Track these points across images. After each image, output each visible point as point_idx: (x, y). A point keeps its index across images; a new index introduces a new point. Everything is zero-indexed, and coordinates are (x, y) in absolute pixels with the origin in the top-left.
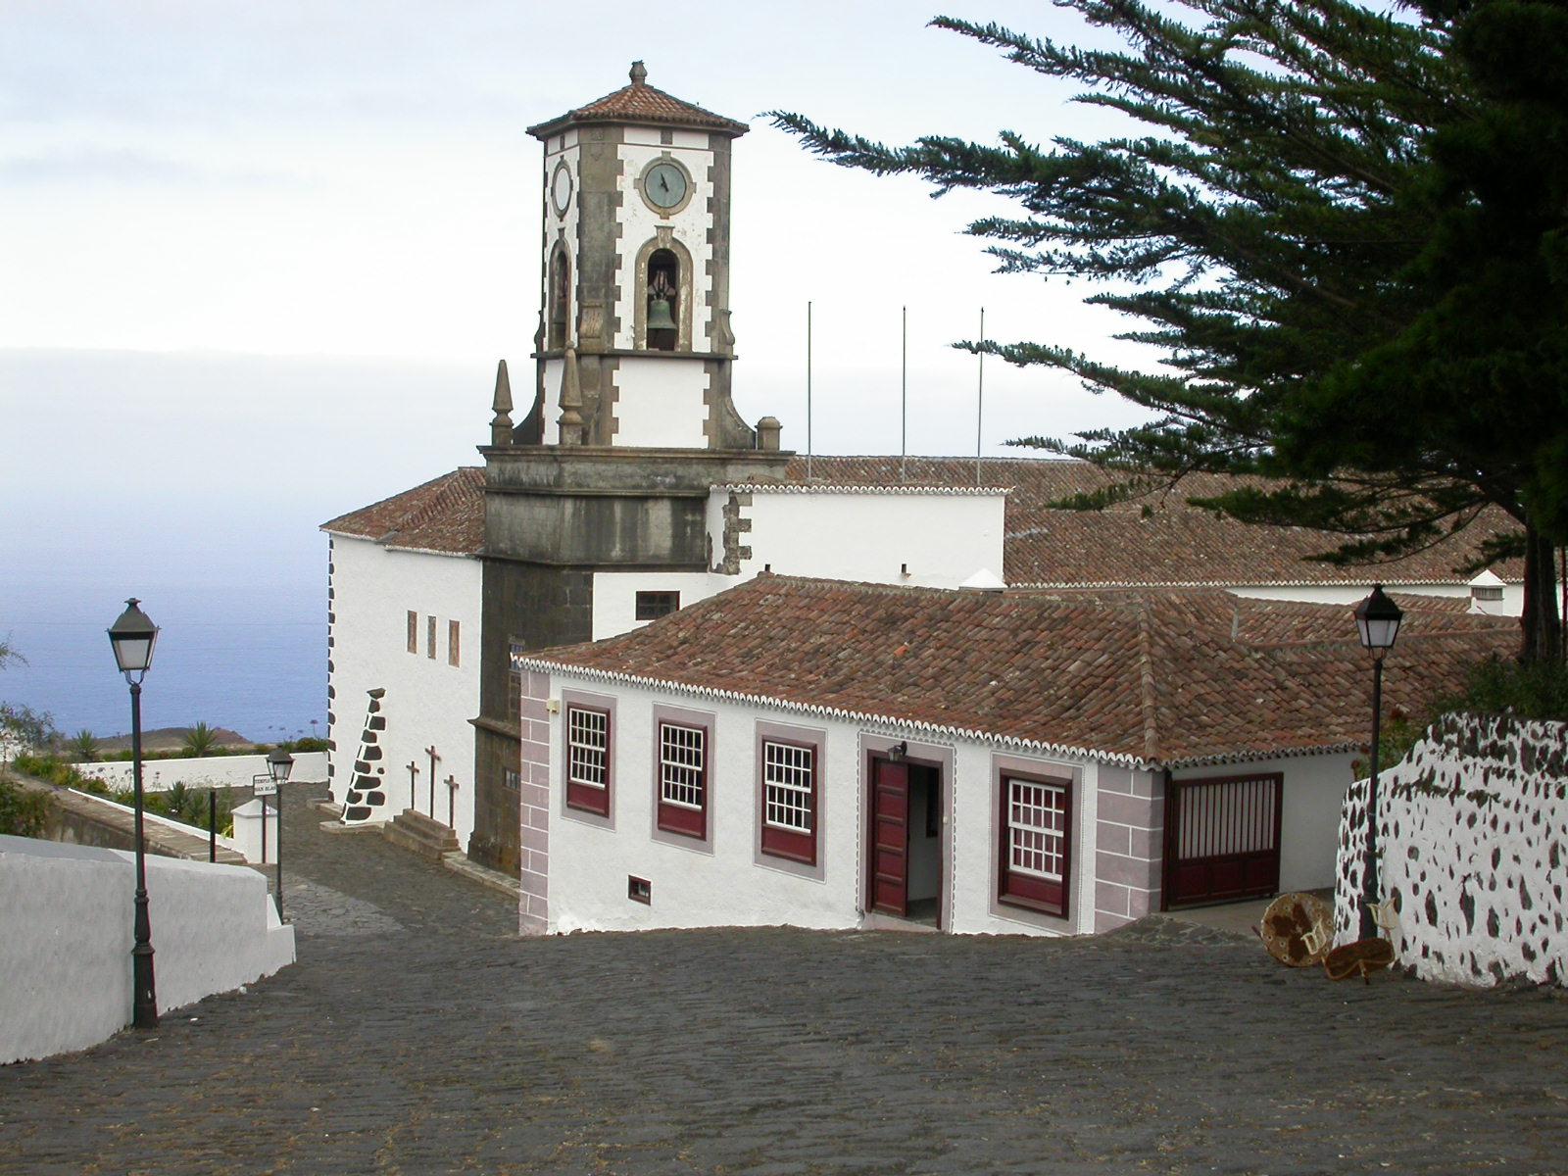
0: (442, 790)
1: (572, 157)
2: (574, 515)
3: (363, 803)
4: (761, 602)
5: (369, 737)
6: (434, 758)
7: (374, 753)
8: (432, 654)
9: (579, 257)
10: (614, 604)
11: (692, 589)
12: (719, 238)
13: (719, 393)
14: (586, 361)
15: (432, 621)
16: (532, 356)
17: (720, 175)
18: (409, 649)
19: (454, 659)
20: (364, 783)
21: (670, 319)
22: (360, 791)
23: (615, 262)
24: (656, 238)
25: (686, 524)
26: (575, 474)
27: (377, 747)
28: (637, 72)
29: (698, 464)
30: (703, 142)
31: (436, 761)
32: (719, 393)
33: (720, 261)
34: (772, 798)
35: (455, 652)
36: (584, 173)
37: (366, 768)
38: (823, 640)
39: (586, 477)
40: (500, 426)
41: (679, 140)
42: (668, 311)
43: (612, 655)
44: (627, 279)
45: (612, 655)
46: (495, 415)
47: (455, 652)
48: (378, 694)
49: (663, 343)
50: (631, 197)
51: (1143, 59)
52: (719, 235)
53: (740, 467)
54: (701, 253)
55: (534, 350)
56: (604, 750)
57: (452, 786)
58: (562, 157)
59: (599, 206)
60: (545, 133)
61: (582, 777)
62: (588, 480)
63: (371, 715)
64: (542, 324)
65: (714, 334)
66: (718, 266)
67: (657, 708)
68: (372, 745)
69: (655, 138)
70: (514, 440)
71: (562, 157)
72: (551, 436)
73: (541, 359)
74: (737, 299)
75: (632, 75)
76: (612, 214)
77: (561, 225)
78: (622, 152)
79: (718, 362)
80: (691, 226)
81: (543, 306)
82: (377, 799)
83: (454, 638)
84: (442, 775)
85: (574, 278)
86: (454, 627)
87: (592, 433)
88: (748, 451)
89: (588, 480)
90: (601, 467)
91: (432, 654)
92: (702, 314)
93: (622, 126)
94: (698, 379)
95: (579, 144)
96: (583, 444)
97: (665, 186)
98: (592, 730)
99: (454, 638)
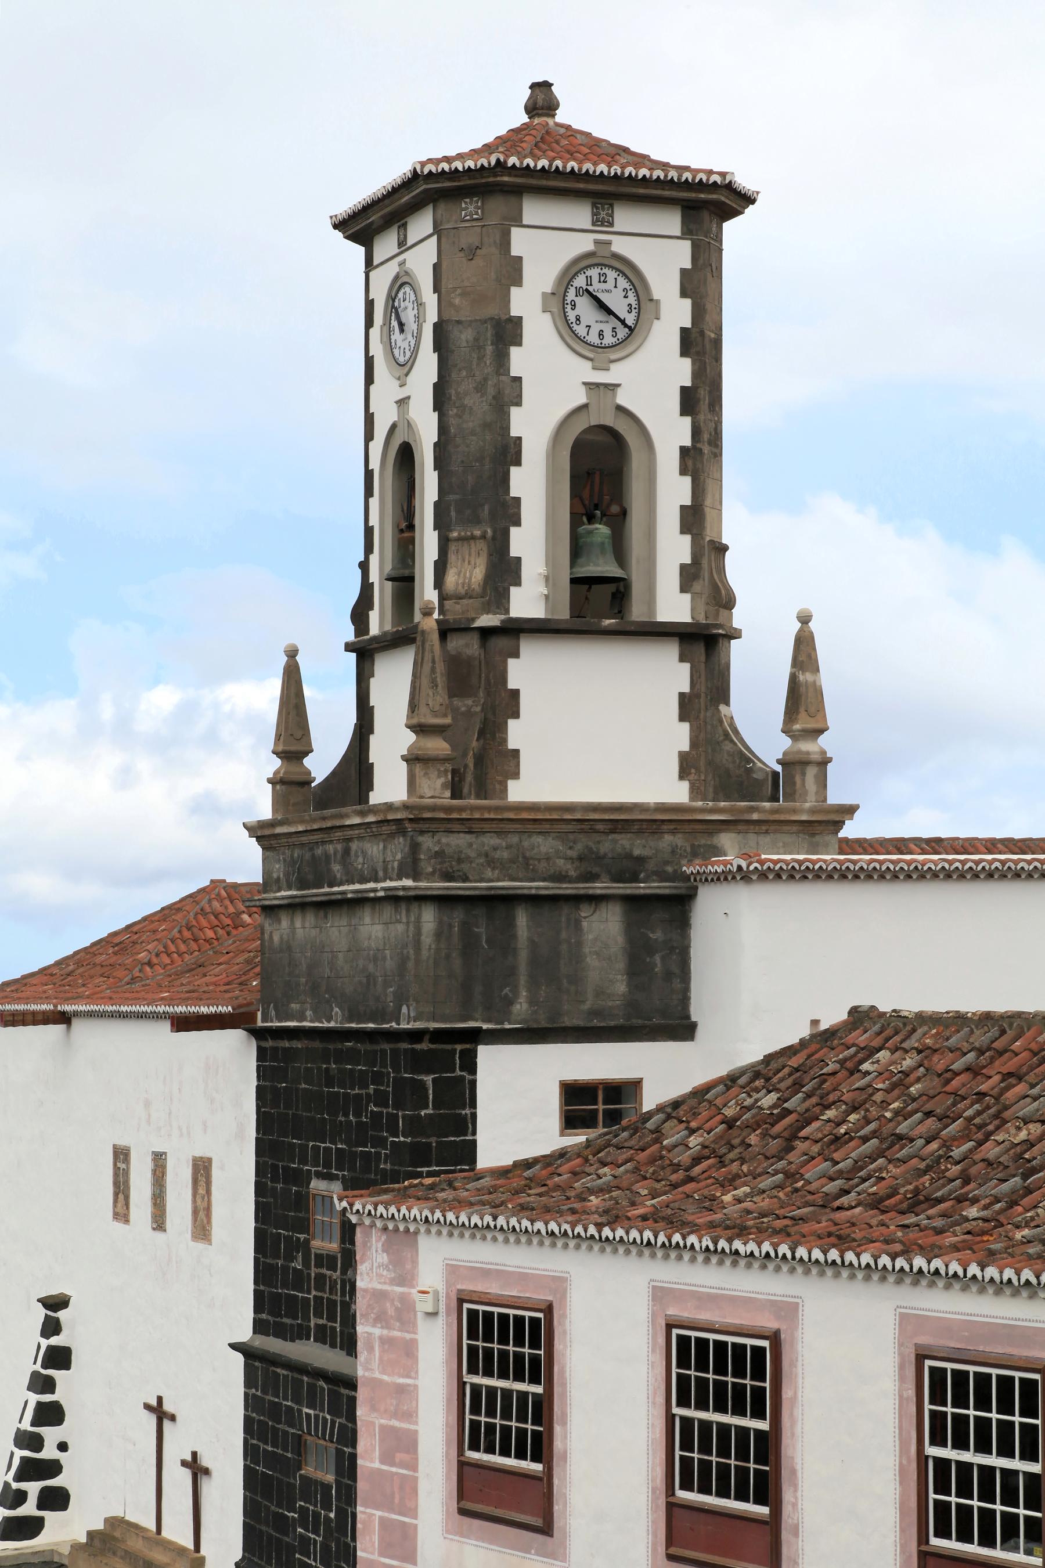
0: (177, 1480)
1: (422, 260)
2: (438, 935)
3: (29, 1509)
4: (866, 1066)
5: (42, 1384)
6: (160, 1413)
7: (50, 1414)
8: (159, 1223)
9: (440, 448)
10: (517, 1101)
11: (660, 1072)
12: (704, 406)
13: (705, 701)
14: (456, 643)
15: (159, 1160)
16: (349, 647)
17: (702, 282)
18: (116, 1216)
19: (202, 1229)
20: (30, 1470)
21: (610, 556)
22: (23, 1486)
23: (510, 452)
24: (585, 407)
25: (650, 948)
26: (439, 855)
27: (991, 1454)
28: (542, 100)
29: (673, 832)
30: (671, 221)
31: (166, 1423)
32: (705, 701)
33: (706, 449)
34: (942, 1487)
35: (202, 1215)
36: (446, 284)
37: (34, 1442)
38: (1023, 1135)
39: (460, 861)
40: (290, 785)
41: (626, 218)
42: (608, 542)
43: (534, 1192)
44: (532, 484)
45: (534, 1192)
46: (277, 762)
47: (202, 1215)
48: (56, 1303)
49: (600, 606)
50: (539, 330)
51: (679, 793)
52: (701, 399)
53: (752, 837)
54: (670, 432)
55: (349, 633)
56: (539, 1389)
57: (197, 1469)
58: (402, 264)
59: (477, 346)
60: (362, 225)
61: (490, 1450)
62: (465, 866)
63: (45, 1343)
64: (366, 588)
65: (697, 586)
66: (701, 458)
67: (659, 1294)
68: (47, 1398)
69: (580, 214)
70: (315, 815)
71: (402, 264)
72: (390, 785)
73: (365, 653)
74: (735, 524)
75: (532, 109)
76: (502, 359)
77: (401, 394)
78: (520, 242)
79: (705, 643)
80: (650, 383)
81: (369, 549)
82: (56, 1500)
83: (202, 1191)
84: (176, 1451)
85: (447, 480)
86: (202, 1169)
87: (469, 778)
88: (760, 804)
89: (465, 866)
90: (491, 841)
91: (159, 1223)
92: (673, 549)
93: (517, 192)
94: (669, 673)
95: (437, 230)
96: (453, 796)
97: (603, 309)
98: (509, 1355)
99: (202, 1191)
